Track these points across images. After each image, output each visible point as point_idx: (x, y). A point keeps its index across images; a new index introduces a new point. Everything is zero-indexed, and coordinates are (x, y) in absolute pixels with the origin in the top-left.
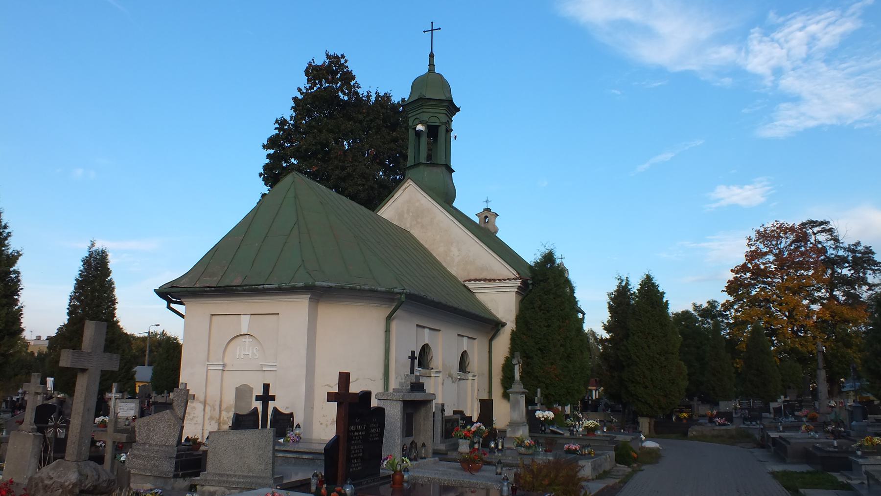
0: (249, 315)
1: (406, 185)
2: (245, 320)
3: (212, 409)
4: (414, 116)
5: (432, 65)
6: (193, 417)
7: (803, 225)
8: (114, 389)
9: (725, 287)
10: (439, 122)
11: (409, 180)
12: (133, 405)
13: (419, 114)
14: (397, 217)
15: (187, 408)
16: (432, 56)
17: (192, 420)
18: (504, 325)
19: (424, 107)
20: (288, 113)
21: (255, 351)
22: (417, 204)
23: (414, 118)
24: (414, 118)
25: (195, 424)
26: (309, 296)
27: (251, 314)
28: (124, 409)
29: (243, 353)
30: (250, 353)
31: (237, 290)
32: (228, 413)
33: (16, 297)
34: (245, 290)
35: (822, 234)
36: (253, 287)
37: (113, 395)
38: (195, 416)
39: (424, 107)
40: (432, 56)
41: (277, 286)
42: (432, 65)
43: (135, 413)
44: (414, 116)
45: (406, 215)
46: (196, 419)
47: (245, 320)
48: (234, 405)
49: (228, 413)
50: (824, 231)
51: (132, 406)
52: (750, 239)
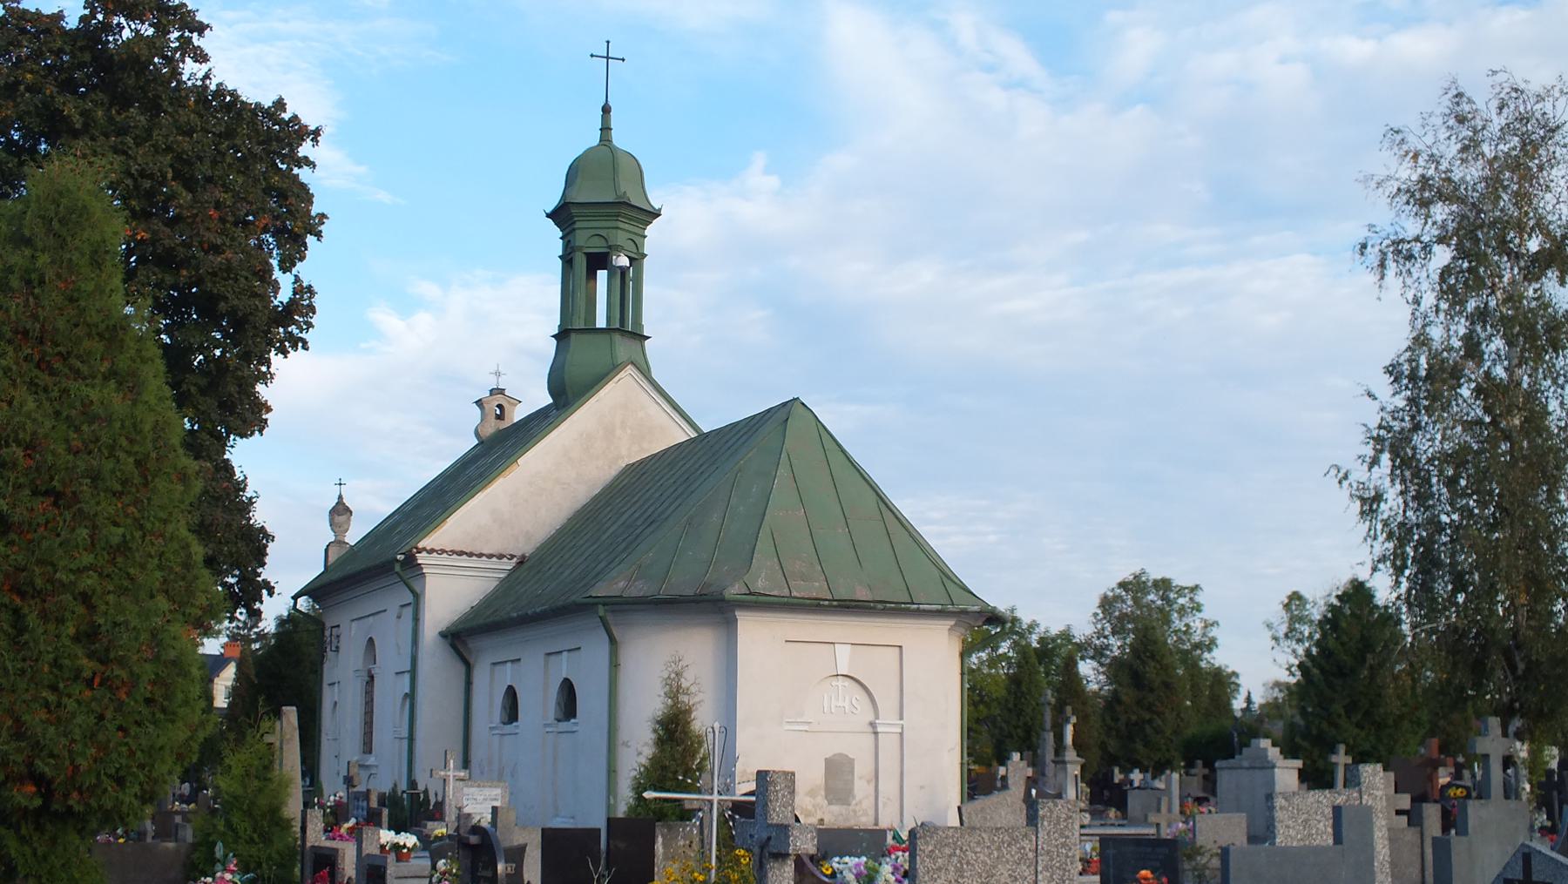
1: (622, 374)
2: (843, 652)
4: (630, 232)
5: (606, 129)
8: (452, 761)
9: (286, 357)
12: (498, 791)
15: (355, 853)
16: (606, 110)
18: (599, 830)
21: (854, 702)
26: (953, 623)
28: (475, 799)
30: (847, 704)
31: (874, 608)
33: (1330, 615)
34: (819, 605)
37: (451, 773)
40: (606, 110)
41: (940, 607)
42: (606, 129)
44: (630, 232)
45: (618, 432)
47: (843, 652)
51: (495, 793)
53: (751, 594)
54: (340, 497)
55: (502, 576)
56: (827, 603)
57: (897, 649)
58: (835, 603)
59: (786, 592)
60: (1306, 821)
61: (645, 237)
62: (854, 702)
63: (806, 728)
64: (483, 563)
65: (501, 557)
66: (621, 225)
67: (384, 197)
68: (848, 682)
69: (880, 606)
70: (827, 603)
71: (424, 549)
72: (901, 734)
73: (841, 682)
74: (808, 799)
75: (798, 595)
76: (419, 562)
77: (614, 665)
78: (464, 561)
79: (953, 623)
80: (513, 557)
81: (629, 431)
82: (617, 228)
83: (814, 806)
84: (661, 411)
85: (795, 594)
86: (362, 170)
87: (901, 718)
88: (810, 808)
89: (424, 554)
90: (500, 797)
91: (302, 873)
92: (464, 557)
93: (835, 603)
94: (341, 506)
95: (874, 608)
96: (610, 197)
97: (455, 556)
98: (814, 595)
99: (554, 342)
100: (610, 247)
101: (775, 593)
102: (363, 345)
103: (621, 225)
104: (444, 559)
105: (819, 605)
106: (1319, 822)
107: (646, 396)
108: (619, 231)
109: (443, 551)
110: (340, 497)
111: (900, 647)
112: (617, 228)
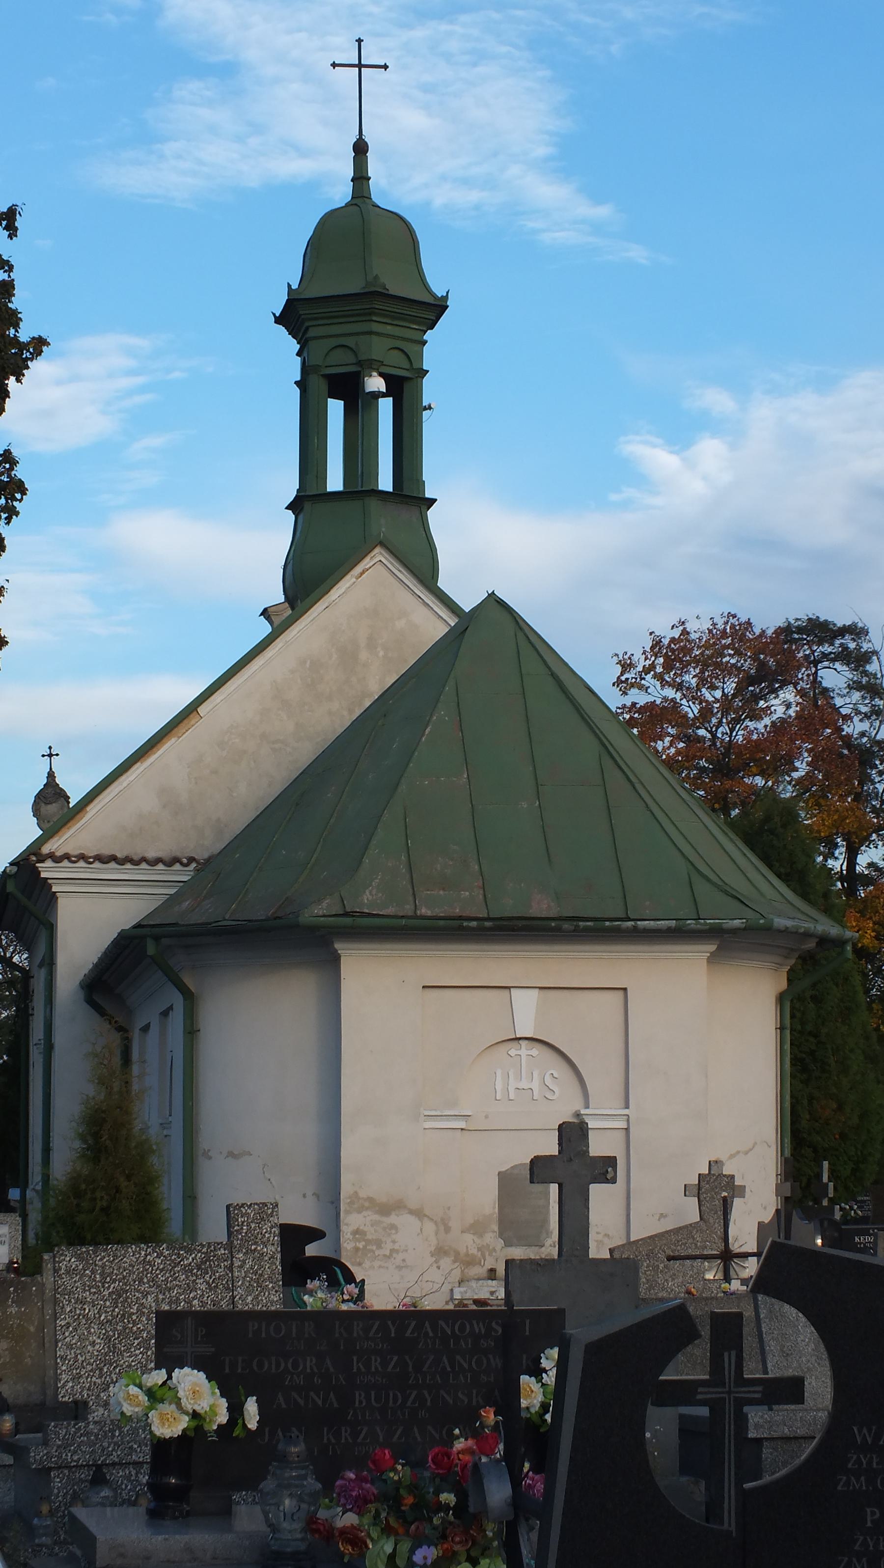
0: (537, 990)
1: (366, 563)
3: (442, 1228)
5: (360, 178)
6: (392, 1251)
7: (786, 632)
10: (407, 366)
11: (378, 550)
13: (357, 334)
14: (335, 656)
16: (360, 148)
17: (388, 1257)
19: (374, 318)
20: (14, 283)
21: (548, 1080)
22: (400, 624)
23: (334, 342)
24: (334, 342)
25: (399, 1268)
26: (713, 948)
27: (540, 988)
29: (513, 1084)
30: (535, 1085)
31: (558, 929)
32: (481, 1236)
35: (837, 665)
36: (607, 923)
38: (396, 1247)
39: (374, 318)
40: (360, 148)
41: (673, 923)
42: (360, 178)
43: (10, 1253)
45: (364, 655)
46: (399, 1257)
48: (496, 1216)
49: (481, 1236)
50: (845, 656)
52: (626, 666)
53: (346, 914)
54: (51, 775)
55: (172, 891)
56: (474, 924)
57: (621, 993)
58: (488, 924)
59: (408, 909)
60: (119, 1293)
61: (425, 343)
62: (548, 1080)
63: (462, 1124)
64: (143, 873)
65: (170, 862)
66: (375, 327)
67: (638, 254)
68: (536, 1051)
69: (566, 926)
70: (474, 924)
71: (52, 856)
72: (627, 1130)
73: (525, 1050)
74: (469, 1238)
75: (429, 913)
76: (43, 875)
77: (191, 1032)
78: (112, 872)
79: (713, 948)
80: (191, 860)
81: (381, 654)
82: (371, 333)
83: (479, 1249)
84: (434, 618)
85: (424, 911)
86: (603, 212)
87: (627, 1107)
88: (474, 1251)
89: (49, 863)
90: (7, 1240)
91: (209, 1352)
92: (113, 865)
93: (488, 924)
94: (50, 790)
95: (558, 929)
96: (354, 286)
97: (97, 865)
98: (457, 911)
99: (290, 516)
100: (359, 363)
101: (390, 911)
102: (614, 497)
103: (375, 327)
104: (81, 870)
105: (461, 928)
106: (146, 1295)
107: (409, 596)
108: (375, 338)
109: (82, 857)
110: (51, 775)
111: (625, 989)
112: (371, 333)
